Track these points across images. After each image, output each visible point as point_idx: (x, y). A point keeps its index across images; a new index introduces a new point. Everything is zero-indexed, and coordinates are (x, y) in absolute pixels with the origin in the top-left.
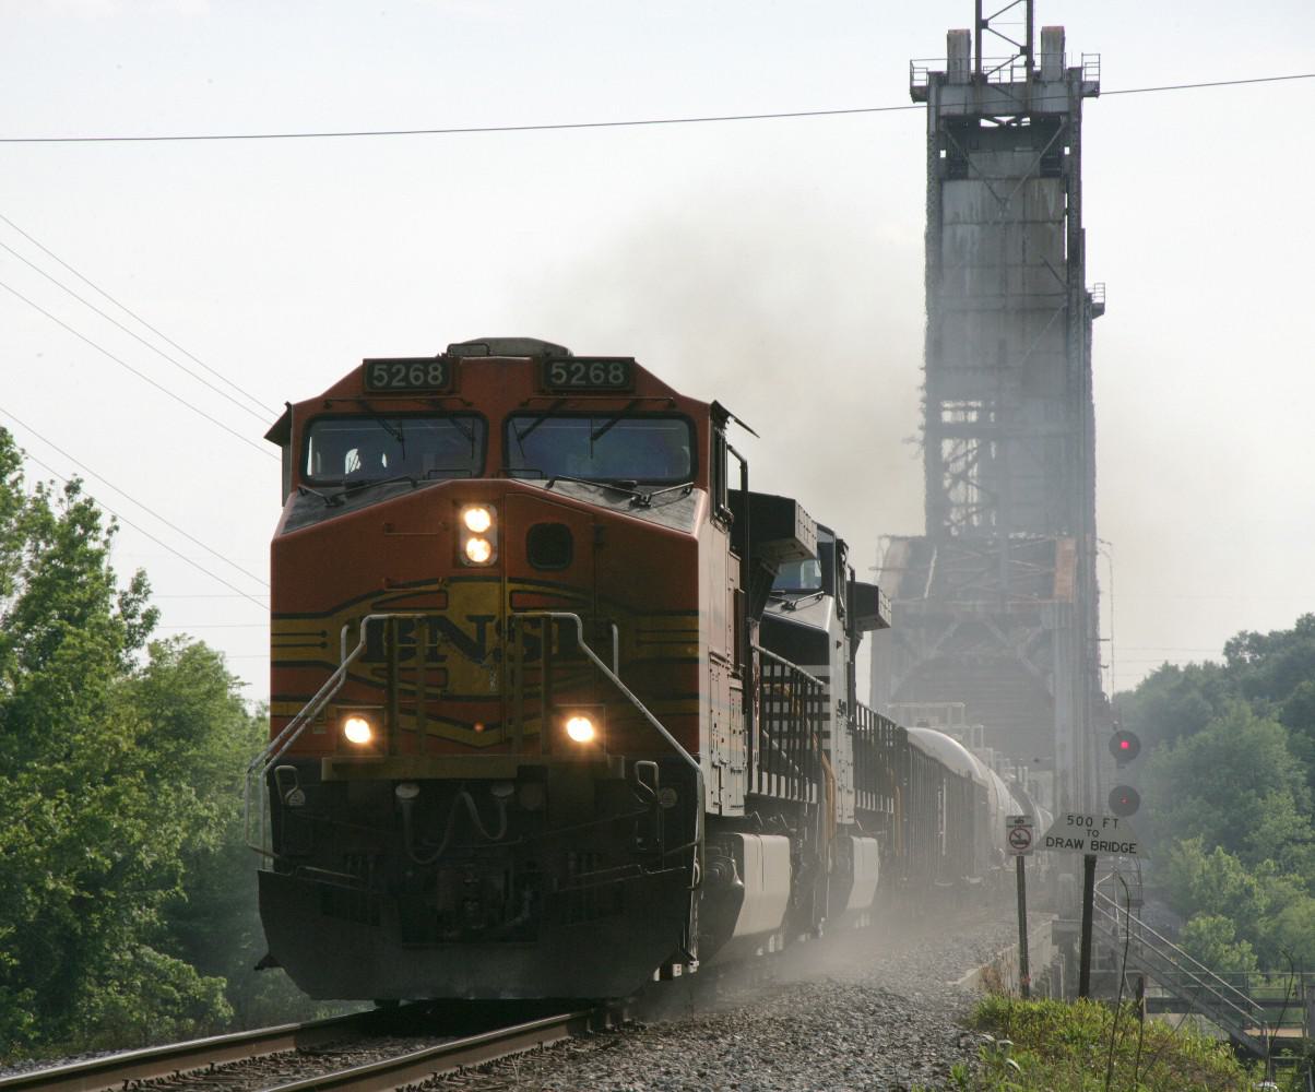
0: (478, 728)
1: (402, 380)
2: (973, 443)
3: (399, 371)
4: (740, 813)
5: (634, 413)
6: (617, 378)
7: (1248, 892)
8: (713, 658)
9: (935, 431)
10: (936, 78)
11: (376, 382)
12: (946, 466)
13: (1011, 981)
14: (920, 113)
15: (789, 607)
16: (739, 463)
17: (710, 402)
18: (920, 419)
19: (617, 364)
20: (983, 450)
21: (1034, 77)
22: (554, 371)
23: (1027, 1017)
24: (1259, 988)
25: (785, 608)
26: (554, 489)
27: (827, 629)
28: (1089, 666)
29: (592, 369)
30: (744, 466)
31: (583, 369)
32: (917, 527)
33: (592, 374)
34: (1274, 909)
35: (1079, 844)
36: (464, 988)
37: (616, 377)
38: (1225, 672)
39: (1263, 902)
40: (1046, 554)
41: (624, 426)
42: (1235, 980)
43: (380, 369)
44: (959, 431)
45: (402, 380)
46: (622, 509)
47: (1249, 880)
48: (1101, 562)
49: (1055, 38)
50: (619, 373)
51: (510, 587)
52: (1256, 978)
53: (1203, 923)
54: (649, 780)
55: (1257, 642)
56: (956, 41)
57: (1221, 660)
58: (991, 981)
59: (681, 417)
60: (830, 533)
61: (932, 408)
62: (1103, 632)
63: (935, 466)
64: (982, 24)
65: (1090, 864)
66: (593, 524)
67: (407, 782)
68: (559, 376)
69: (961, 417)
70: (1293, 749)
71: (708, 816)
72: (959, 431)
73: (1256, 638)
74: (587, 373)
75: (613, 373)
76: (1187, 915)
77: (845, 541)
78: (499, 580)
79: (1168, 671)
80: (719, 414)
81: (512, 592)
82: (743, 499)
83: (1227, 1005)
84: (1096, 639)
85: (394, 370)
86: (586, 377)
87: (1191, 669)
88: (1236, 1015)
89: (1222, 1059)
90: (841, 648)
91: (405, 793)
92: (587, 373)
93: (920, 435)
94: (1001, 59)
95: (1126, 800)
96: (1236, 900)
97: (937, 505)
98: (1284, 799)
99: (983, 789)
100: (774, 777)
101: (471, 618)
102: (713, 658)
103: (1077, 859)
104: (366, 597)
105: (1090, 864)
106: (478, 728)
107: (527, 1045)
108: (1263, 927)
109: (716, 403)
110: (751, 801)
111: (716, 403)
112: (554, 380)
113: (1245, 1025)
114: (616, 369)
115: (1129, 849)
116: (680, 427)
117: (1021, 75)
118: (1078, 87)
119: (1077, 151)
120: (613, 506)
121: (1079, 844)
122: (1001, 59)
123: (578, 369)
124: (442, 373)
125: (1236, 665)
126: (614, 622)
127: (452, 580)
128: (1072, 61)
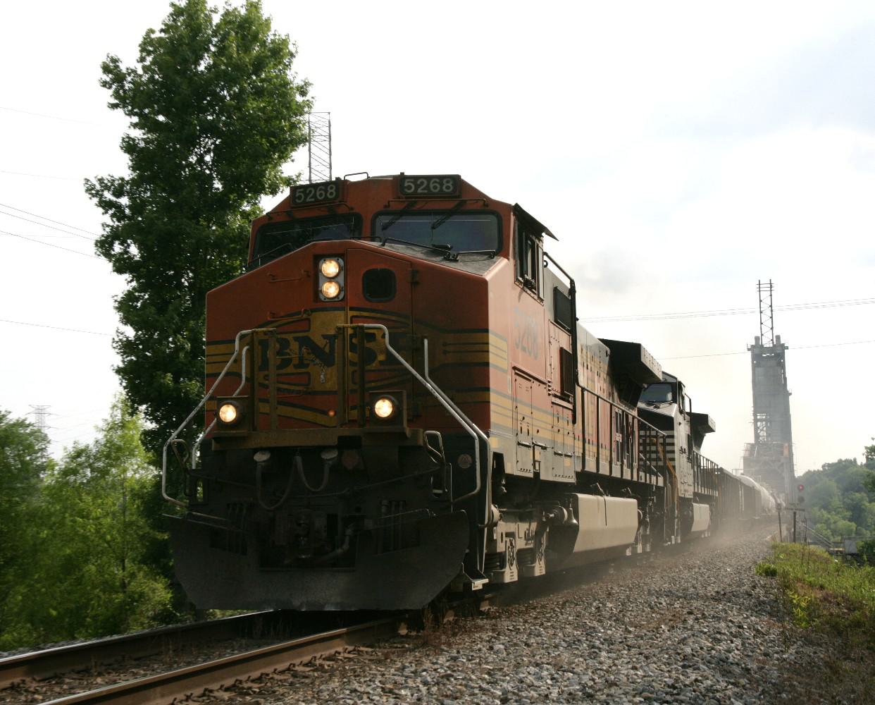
0: (332, 413)
1: (312, 198)
2: (764, 423)
3: (310, 191)
4: (692, 497)
5: (459, 210)
6: (448, 188)
7: (829, 519)
8: (517, 371)
9: (756, 421)
10: (752, 346)
11: (297, 201)
12: (759, 428)
13: (778, 540)
14: (750, 353)
15: (657, 407)
16: (569, 281)
17: (513, 204)
18: (753, 418)
19: (449, 179)
20: (766, 424)
21: (774, 345)
22: (406, 184)
23: (783, 547)
24: (832, 540)
25: (655, 407)
26: (385, 247)
27: (673, 416)
28: (792, 471)
29: (432, 182)
30: (690, 400)
31: (426, 182)
32: (753, 441)
33: (431, 186)
34: (835, 522)
35: (792, 509)
36: (300, 602)
37: (448, 188)
38: (822, 472)
39: (832, 521)
40: (782, 446)
41: (456, 219)
42: (827, 538)
43: (300, 192)
44: (761, 420)
45: (312, 198)
46: (438, 262)
47: (829, 516)
48: (793, 448)
49: (778, 338)
50: (450, 185)
51: (351, 313)
52: (831, 537)
53: (819, 526)
54: (435, 444)
55: (829, 465)
56: (757, 339)
57: (821, 469)
58: (773, 539)
59: (493, 213)
60: (676, 379)
61: (755, 415)
62: (795, 463)
63: (756, 428)
64: (762, 335)
65: (795, 513)
66: (411, 269)
67: (262, 450)
68: (409, 188)
69: (761, 417)
70: (838, 488)
71: (680, 498)
72: (761, 420)
73: (828, 464)
74: (428, 185)
75: (446, 185)
76: (815, 524)
77: (682, 382)
78: (343, 309)
79: (809, 471)
80: (638, 346)
81: (352, 317)
82: (690, 414)
83: (826, 544)
84: (793, 465)
85: (308, 191)
86: (428, 187)
87: (814, 471)
88: (827, 545)
89: (826, 555)
90: (682, 425)
91: (260, 457)
92: (428, 185)
93: (753, 421)
94: (767, 342)
95: (801, 500)
96: (826, 521)
97: (757, 436)
98: (836, 499)
99: (759, 492)
100: (648, 475)
101: (325, 337)
102: (517, 371)
103: (791, 513)
104: (291, 333)
105: (795, 513)
106: (332, 413)
107: (256, 670)
108: (832, 526)
109: (517, 205)
110: (695, 494)
111: (517, 205)
112: (406, 190)
113: (830, 547)
114: (448, 182)
115: (803, 510)
116: (492, 219)
117: (771, 345)
118: (784, 347)
119: (784, 361)
120: (429, 259)
121: (792, 509)
122: (767, 342)
123: (422, 183)
124: (335, 191)
125: (824, 470)
126: (426, 337)
127: (313, 310)
128: (782, 343)
